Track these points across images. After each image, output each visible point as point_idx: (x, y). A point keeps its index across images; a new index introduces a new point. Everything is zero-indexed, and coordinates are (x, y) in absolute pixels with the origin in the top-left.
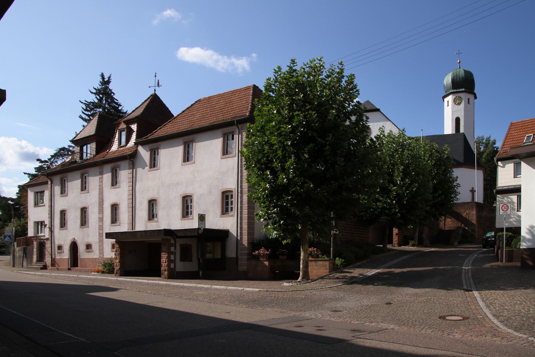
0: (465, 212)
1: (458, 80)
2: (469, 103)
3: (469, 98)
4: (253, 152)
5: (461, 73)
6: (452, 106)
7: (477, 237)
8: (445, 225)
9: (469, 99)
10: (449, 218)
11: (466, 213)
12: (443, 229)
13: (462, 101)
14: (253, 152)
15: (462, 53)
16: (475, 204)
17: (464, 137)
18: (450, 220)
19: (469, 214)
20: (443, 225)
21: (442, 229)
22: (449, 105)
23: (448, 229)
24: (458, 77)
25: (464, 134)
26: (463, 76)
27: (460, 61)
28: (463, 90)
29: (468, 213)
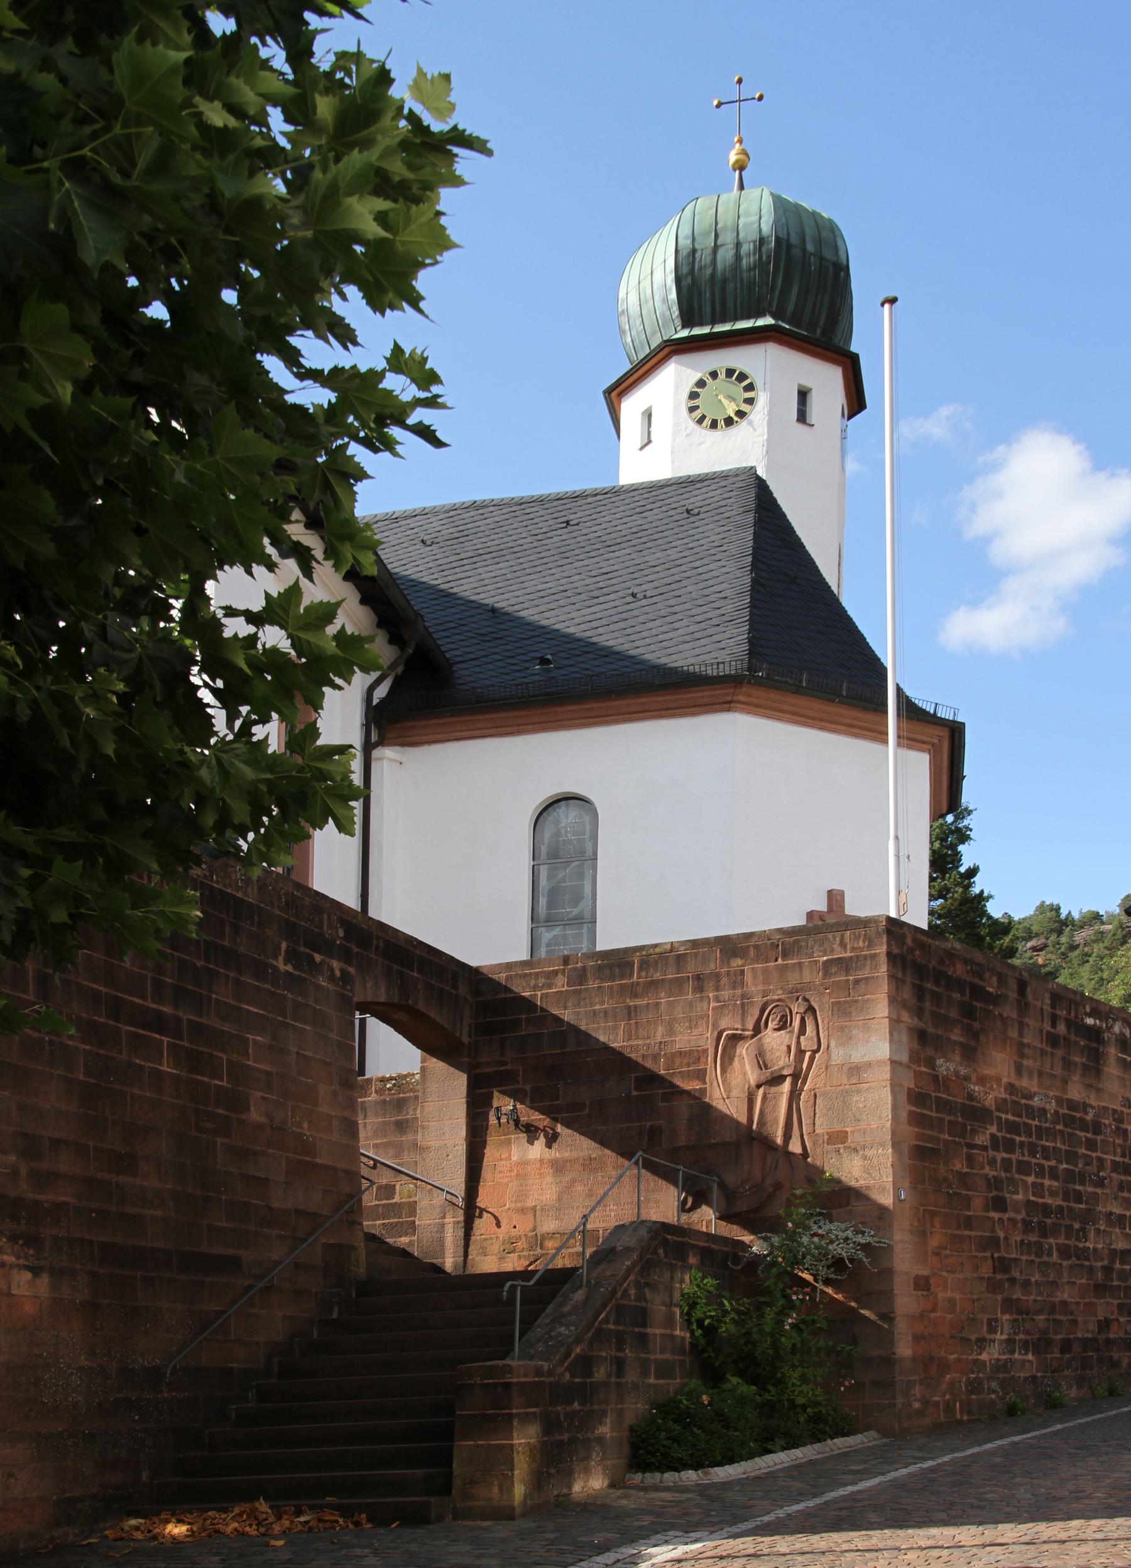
0: (744, 1051)
1: (726, 255)
2: (802, 417)
3: (807, 383)
4: (993, 1396)
5: (755, 209)
6: (674, 438)
7: (904, 1349)
8: (471, 1211)
9: (803, 395)
10: (531, 1131)
11: (762, 1062)
12: (449, 1262)
13: (750, 401)
14: (993, 1396)
15: (761, 98)
16: (881, 949)
17: (758, 497)
18: (537, 1150)
19: (798, 1076)
20: (453, 1220)
21: (438, 1270)
22: (653, 438)
23: (512, 1264)
24: (727, 238)
25: (762, 486)
26: (766, 228)
27: (744, 152)
28: (768, 321)
29: (782, 1061)
